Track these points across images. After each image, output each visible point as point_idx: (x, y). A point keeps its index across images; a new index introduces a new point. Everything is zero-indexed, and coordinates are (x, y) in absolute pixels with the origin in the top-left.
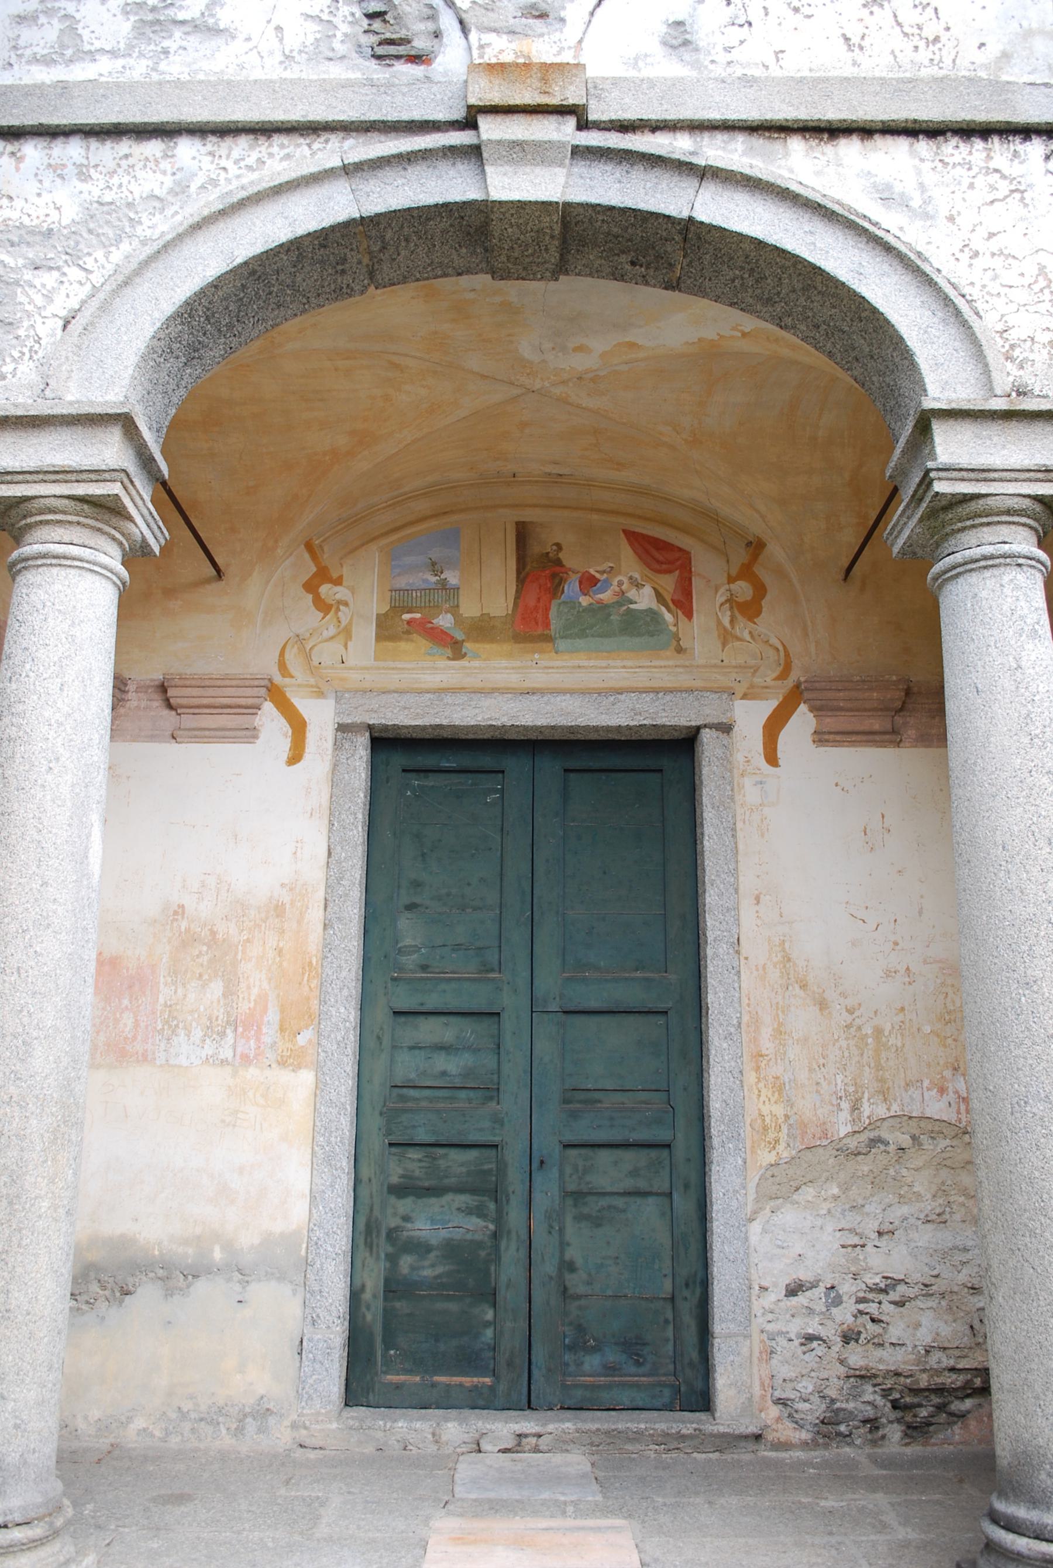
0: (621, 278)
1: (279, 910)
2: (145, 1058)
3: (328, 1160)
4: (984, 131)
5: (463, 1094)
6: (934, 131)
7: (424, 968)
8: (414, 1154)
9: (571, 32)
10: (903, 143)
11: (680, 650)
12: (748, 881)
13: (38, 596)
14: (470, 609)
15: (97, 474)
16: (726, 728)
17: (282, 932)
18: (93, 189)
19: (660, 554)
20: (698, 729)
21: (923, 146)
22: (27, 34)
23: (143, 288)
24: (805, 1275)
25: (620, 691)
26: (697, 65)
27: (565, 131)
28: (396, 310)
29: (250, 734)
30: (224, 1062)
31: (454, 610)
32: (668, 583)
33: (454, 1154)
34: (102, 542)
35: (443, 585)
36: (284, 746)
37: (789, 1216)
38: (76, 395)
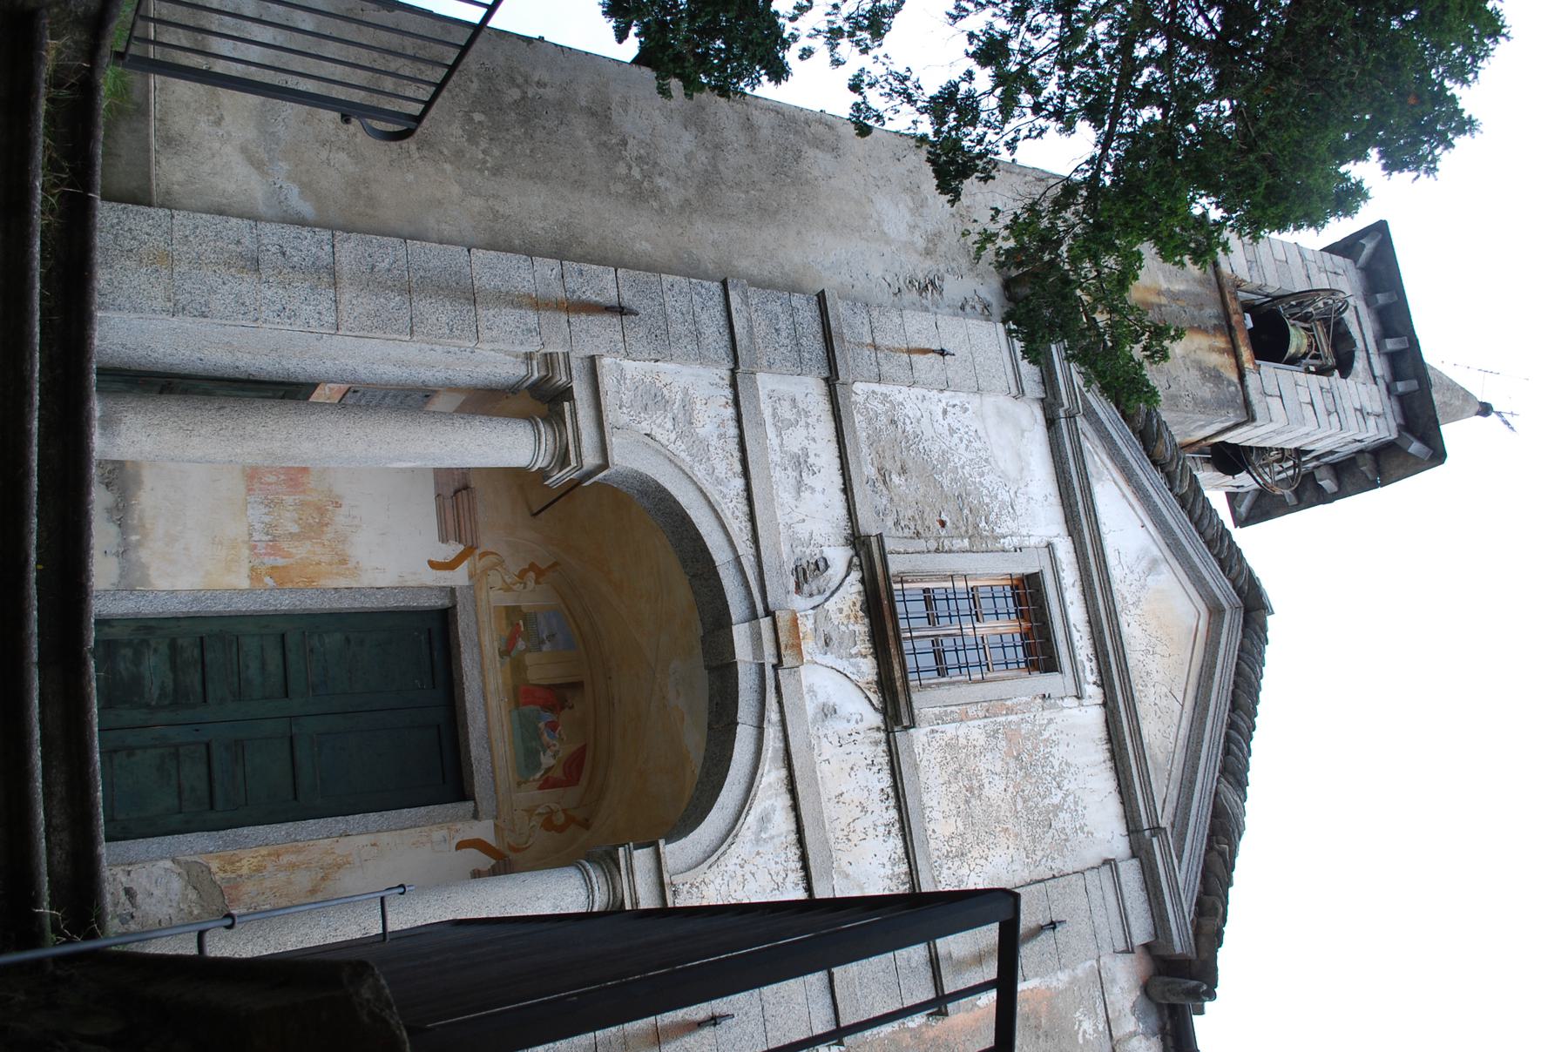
0: (711, 700)
1: (343, 562)
2: (250, 490)
3: (196, 599)
4: (805, 867)
5: (236, 679)
6: (801, 842)
7: (311, 650)
8: (197, 652)
9: (819, 658)
10: (793, 827)
11: (519, 784)
12: (385, 838)
13: (520, 431)
14: (529, 659)
15: (579, 455)
16: (476, 816)
17: (330, 564)
18: (714, 442)
19: (574, 769)
20: (474, 799)
21: (793, 837)
22: (786, 404)
23: (670, 469)
24: (139, 898)
25: (491, 750)
26: (815, 721)
27: (770, 660)
28: (682, 592)
29: (444, 539)
30: (251, 535)
31: (528, 650)
32: (558, 773)
33: (197, 678)
34: (548, 458)
35: (543, 642)
36: (439, 559)
37: (177, 884)
38: (615, 442)
